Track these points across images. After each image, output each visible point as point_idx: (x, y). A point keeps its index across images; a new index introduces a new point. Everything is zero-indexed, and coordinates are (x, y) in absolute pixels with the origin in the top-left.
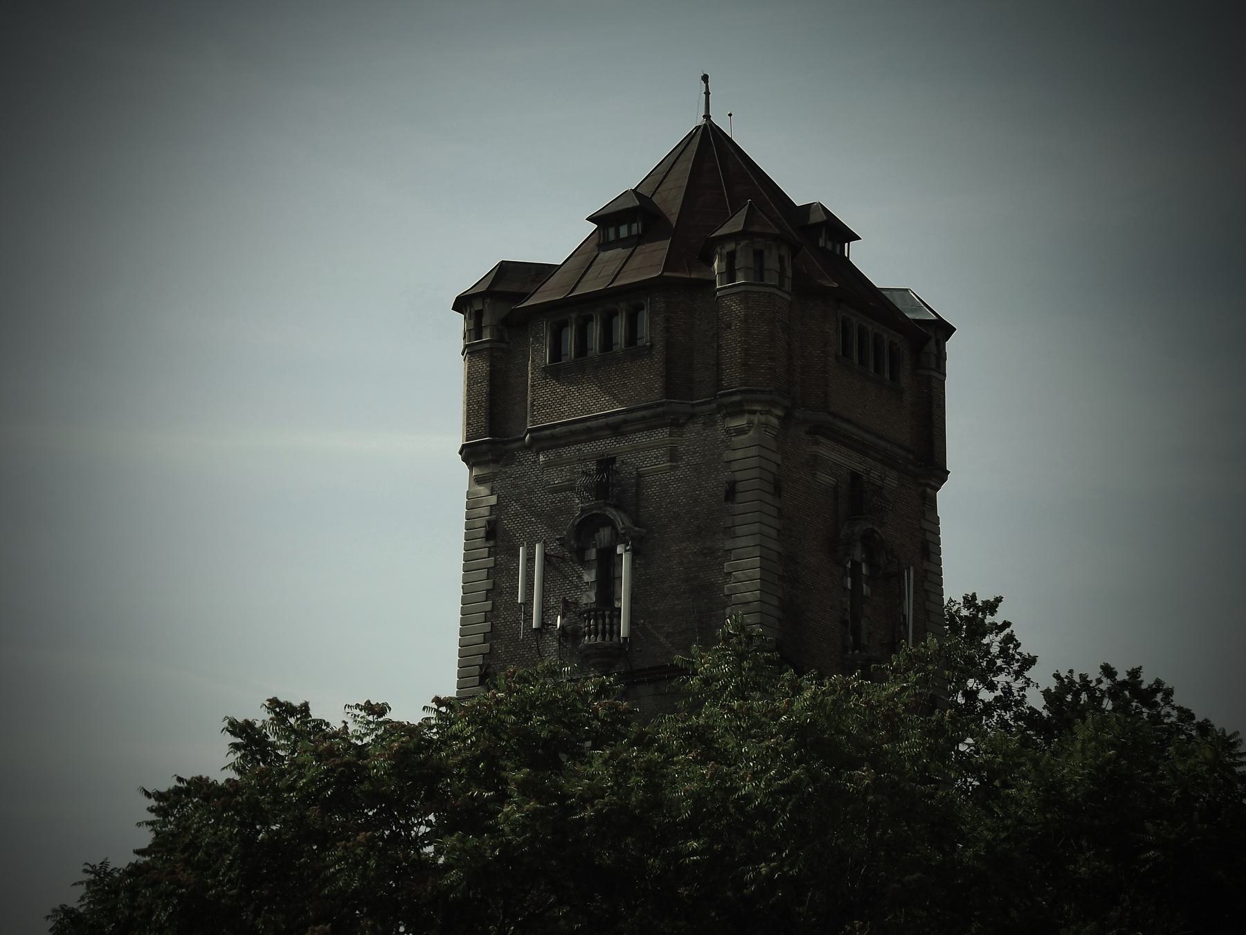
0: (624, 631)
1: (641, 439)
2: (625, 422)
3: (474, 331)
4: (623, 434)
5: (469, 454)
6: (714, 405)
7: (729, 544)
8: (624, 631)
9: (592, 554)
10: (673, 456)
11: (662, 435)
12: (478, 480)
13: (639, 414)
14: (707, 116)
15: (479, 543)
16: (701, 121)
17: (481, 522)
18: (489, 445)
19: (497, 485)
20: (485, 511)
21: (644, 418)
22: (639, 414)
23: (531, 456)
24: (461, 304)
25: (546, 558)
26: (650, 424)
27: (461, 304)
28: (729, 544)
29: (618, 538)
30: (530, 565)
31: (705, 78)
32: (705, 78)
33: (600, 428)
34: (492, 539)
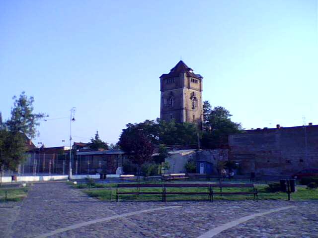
3: (161, 80)
18: (162, 90)
24: (160, 77)
34: (162, 98)
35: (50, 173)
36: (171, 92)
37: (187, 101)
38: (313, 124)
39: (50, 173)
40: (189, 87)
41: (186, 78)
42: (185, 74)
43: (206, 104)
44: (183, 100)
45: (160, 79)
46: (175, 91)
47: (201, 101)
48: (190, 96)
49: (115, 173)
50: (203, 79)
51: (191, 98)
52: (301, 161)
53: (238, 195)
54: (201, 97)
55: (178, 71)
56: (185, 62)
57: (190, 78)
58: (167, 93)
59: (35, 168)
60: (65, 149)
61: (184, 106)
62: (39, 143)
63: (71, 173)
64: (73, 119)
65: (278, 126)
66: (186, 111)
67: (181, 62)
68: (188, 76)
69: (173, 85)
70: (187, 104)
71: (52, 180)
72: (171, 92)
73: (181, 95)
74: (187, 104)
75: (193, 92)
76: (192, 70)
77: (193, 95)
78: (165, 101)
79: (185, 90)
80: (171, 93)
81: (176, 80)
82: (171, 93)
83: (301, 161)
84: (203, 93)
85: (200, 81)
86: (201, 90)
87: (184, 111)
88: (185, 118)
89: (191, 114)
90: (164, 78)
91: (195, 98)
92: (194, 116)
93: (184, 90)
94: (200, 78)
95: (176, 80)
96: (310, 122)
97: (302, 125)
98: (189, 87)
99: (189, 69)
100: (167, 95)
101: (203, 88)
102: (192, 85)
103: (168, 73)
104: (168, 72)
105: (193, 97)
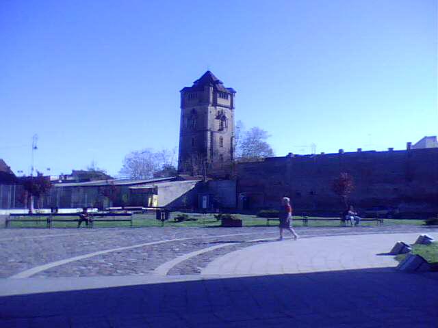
18: (183, 106)
24: (181, 91)
34: (183, 117)
35: (26, 207)
38: (394, 150)
39: (26, 207)
40: (215, 104)
45: (180, 94)
47: (232, 121)
49: (293, 215)
50: (236, 94)
52: (312, 193)
53: (27, 222)
54: (232, 116)
58: (189, 110)
59: (9, 202)
60: (51, 179)
61: (209, 127)
62: (18, 172)
63: (32, 206)
64: (36, 148)
65: (341, 151)
66: (212, 133)
74: (213, 125)
78: (186, 122)
79: (210, 108)
81: (202, 96)
82: (194, 111)
83: (312, 193)
86: (232, 107)
88: (209, 144)
89: (217, 136)
90: (185, 91)
92: (222, 139)
93: (209, 107)
95: (202, 96)
96: (409, 141)
97: (310, 154)
98: (215, 104)
99: (218, 82)
101: (236, 104)
102: (220, 101)
104: (190, 85)
105: (221, 117)
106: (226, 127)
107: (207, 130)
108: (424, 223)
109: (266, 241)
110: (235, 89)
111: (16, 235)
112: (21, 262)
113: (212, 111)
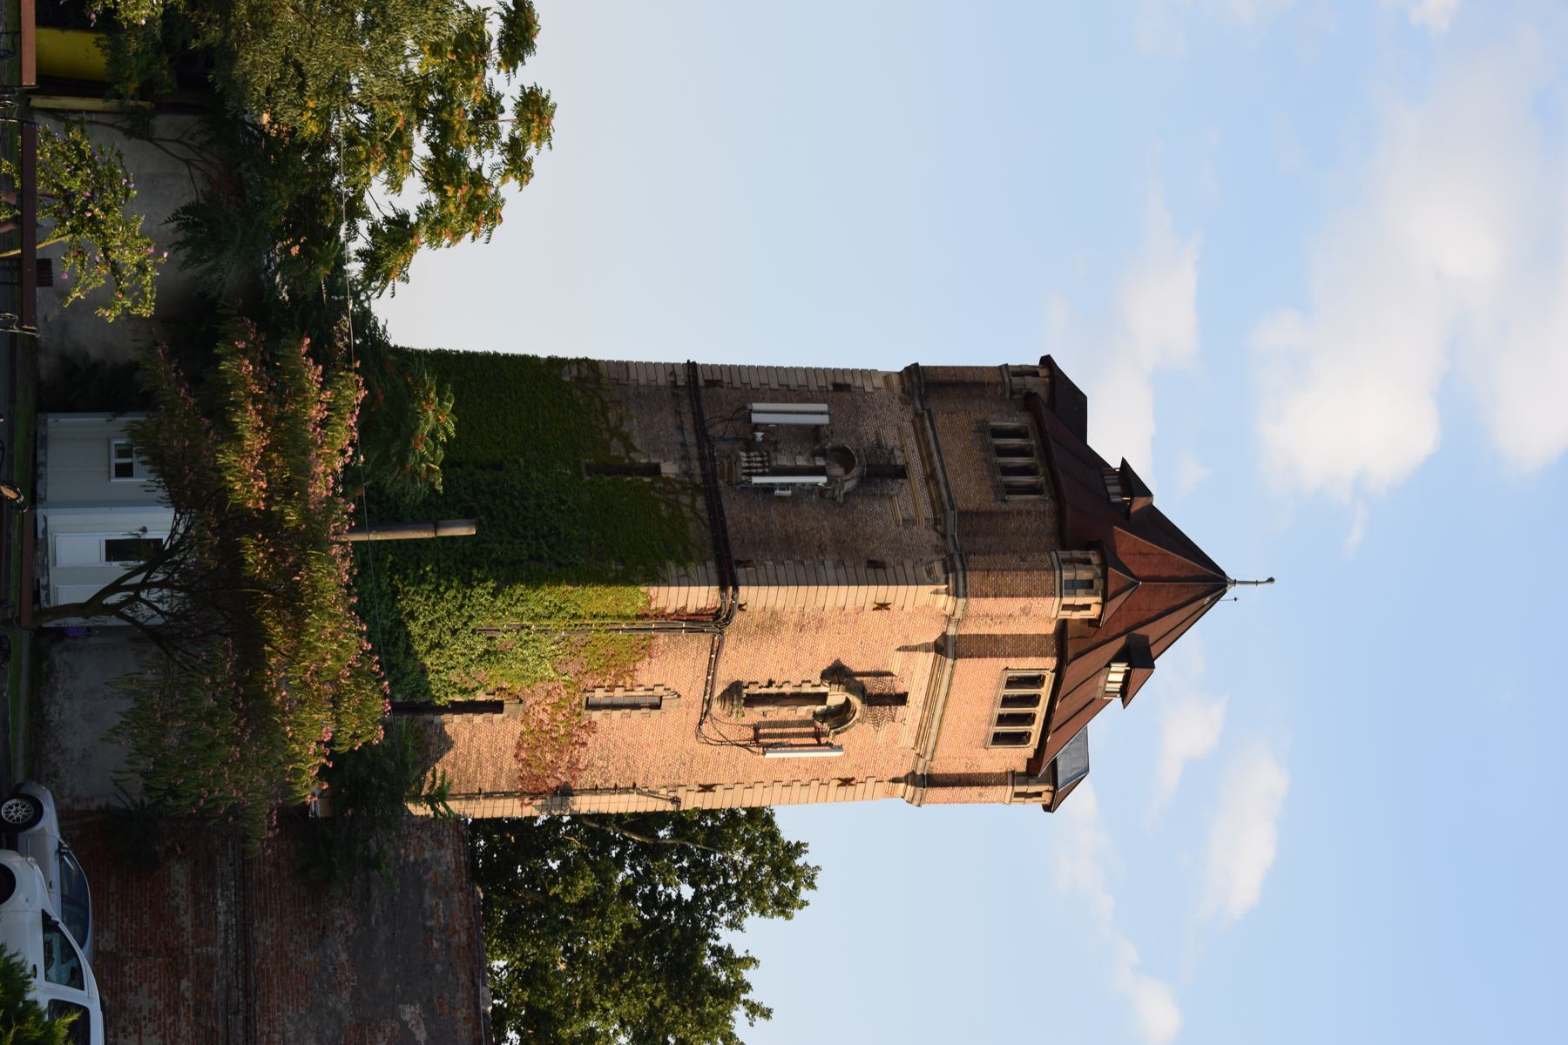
0: (756, 480)
1: (923, 497)
2: (938, 483)
3: (1023, 372)
4: (927, 483)
5: (914, 370)
6: (952, 550)
7: (829, 563)
8: (756, 480)
9: (820, 462)
10: (909, 522)
11: (926, 511)
12: (887, 377)
13: (944, 492)
14: (1235, 582)
15: (831, 379)
16: (1231, 574)
17: (849, 380)
18: (922, 384)
19: (884, 392)
20: (858, 383)
21: (940, 496)
22: (944, 492)
23: (909, 417)
24: (1047, 361)
25: (817, 428)
26: (937, 504)
27: (1047, 361)
28: (829, 563)
29: (831, 480)
30: (814, 414)
31: (1271, 580)
32: (1271, 580)
33: (931, 464)
34: (839, 387)
36: (901, 473)
37: (802, 625)
41: (1038, 614)
42: (1091, 606)
43: (777, 876)
44: (816, 579)
46: (910, 501)
48: (855, 663)
49: (42, 21)
51: (837, 673)
55: (1127, 542)
56: (1220, 614)
57: (1045, 665)
58: (893, 431)
61: (754, 597)
66: (697, 622)
67: (1206, 582)
68: (1064, 643)
69: (971, 490)
70: (771, 624)
71: (138, 107)
72: (901, 473)
73: (875, 570)
74: (771, 624)
75: (901, 699)
76: (1125, 693)
77: (872, 700)
79: (923, 606)
80: (882, 472)
82: (882, 472)
84: (896, 811)
85: (1012, 778)
86: (926, 781)
87: (701, 597)
89: (676, 668)
90: (1044, 404)
91: (840, 716)
93: (925, 591)
94: (1046, 778)
99: (1140, 658)
100: (868, 429)
101: (944, 809)
102: (979, 685)
103: (1090, 443)
104: (1110, 437)
105: (861, 693)
106: (760, 739)
107: (727, 581)
108: (383, 175)
109: (12, 401)
110: (1079, 801)
111: (226, 952)
112: (391, 98)
113: (885, 620)
